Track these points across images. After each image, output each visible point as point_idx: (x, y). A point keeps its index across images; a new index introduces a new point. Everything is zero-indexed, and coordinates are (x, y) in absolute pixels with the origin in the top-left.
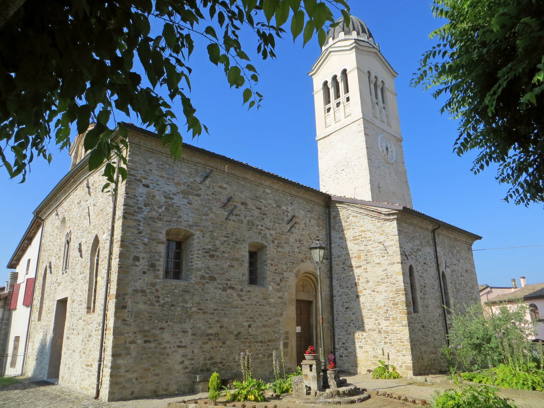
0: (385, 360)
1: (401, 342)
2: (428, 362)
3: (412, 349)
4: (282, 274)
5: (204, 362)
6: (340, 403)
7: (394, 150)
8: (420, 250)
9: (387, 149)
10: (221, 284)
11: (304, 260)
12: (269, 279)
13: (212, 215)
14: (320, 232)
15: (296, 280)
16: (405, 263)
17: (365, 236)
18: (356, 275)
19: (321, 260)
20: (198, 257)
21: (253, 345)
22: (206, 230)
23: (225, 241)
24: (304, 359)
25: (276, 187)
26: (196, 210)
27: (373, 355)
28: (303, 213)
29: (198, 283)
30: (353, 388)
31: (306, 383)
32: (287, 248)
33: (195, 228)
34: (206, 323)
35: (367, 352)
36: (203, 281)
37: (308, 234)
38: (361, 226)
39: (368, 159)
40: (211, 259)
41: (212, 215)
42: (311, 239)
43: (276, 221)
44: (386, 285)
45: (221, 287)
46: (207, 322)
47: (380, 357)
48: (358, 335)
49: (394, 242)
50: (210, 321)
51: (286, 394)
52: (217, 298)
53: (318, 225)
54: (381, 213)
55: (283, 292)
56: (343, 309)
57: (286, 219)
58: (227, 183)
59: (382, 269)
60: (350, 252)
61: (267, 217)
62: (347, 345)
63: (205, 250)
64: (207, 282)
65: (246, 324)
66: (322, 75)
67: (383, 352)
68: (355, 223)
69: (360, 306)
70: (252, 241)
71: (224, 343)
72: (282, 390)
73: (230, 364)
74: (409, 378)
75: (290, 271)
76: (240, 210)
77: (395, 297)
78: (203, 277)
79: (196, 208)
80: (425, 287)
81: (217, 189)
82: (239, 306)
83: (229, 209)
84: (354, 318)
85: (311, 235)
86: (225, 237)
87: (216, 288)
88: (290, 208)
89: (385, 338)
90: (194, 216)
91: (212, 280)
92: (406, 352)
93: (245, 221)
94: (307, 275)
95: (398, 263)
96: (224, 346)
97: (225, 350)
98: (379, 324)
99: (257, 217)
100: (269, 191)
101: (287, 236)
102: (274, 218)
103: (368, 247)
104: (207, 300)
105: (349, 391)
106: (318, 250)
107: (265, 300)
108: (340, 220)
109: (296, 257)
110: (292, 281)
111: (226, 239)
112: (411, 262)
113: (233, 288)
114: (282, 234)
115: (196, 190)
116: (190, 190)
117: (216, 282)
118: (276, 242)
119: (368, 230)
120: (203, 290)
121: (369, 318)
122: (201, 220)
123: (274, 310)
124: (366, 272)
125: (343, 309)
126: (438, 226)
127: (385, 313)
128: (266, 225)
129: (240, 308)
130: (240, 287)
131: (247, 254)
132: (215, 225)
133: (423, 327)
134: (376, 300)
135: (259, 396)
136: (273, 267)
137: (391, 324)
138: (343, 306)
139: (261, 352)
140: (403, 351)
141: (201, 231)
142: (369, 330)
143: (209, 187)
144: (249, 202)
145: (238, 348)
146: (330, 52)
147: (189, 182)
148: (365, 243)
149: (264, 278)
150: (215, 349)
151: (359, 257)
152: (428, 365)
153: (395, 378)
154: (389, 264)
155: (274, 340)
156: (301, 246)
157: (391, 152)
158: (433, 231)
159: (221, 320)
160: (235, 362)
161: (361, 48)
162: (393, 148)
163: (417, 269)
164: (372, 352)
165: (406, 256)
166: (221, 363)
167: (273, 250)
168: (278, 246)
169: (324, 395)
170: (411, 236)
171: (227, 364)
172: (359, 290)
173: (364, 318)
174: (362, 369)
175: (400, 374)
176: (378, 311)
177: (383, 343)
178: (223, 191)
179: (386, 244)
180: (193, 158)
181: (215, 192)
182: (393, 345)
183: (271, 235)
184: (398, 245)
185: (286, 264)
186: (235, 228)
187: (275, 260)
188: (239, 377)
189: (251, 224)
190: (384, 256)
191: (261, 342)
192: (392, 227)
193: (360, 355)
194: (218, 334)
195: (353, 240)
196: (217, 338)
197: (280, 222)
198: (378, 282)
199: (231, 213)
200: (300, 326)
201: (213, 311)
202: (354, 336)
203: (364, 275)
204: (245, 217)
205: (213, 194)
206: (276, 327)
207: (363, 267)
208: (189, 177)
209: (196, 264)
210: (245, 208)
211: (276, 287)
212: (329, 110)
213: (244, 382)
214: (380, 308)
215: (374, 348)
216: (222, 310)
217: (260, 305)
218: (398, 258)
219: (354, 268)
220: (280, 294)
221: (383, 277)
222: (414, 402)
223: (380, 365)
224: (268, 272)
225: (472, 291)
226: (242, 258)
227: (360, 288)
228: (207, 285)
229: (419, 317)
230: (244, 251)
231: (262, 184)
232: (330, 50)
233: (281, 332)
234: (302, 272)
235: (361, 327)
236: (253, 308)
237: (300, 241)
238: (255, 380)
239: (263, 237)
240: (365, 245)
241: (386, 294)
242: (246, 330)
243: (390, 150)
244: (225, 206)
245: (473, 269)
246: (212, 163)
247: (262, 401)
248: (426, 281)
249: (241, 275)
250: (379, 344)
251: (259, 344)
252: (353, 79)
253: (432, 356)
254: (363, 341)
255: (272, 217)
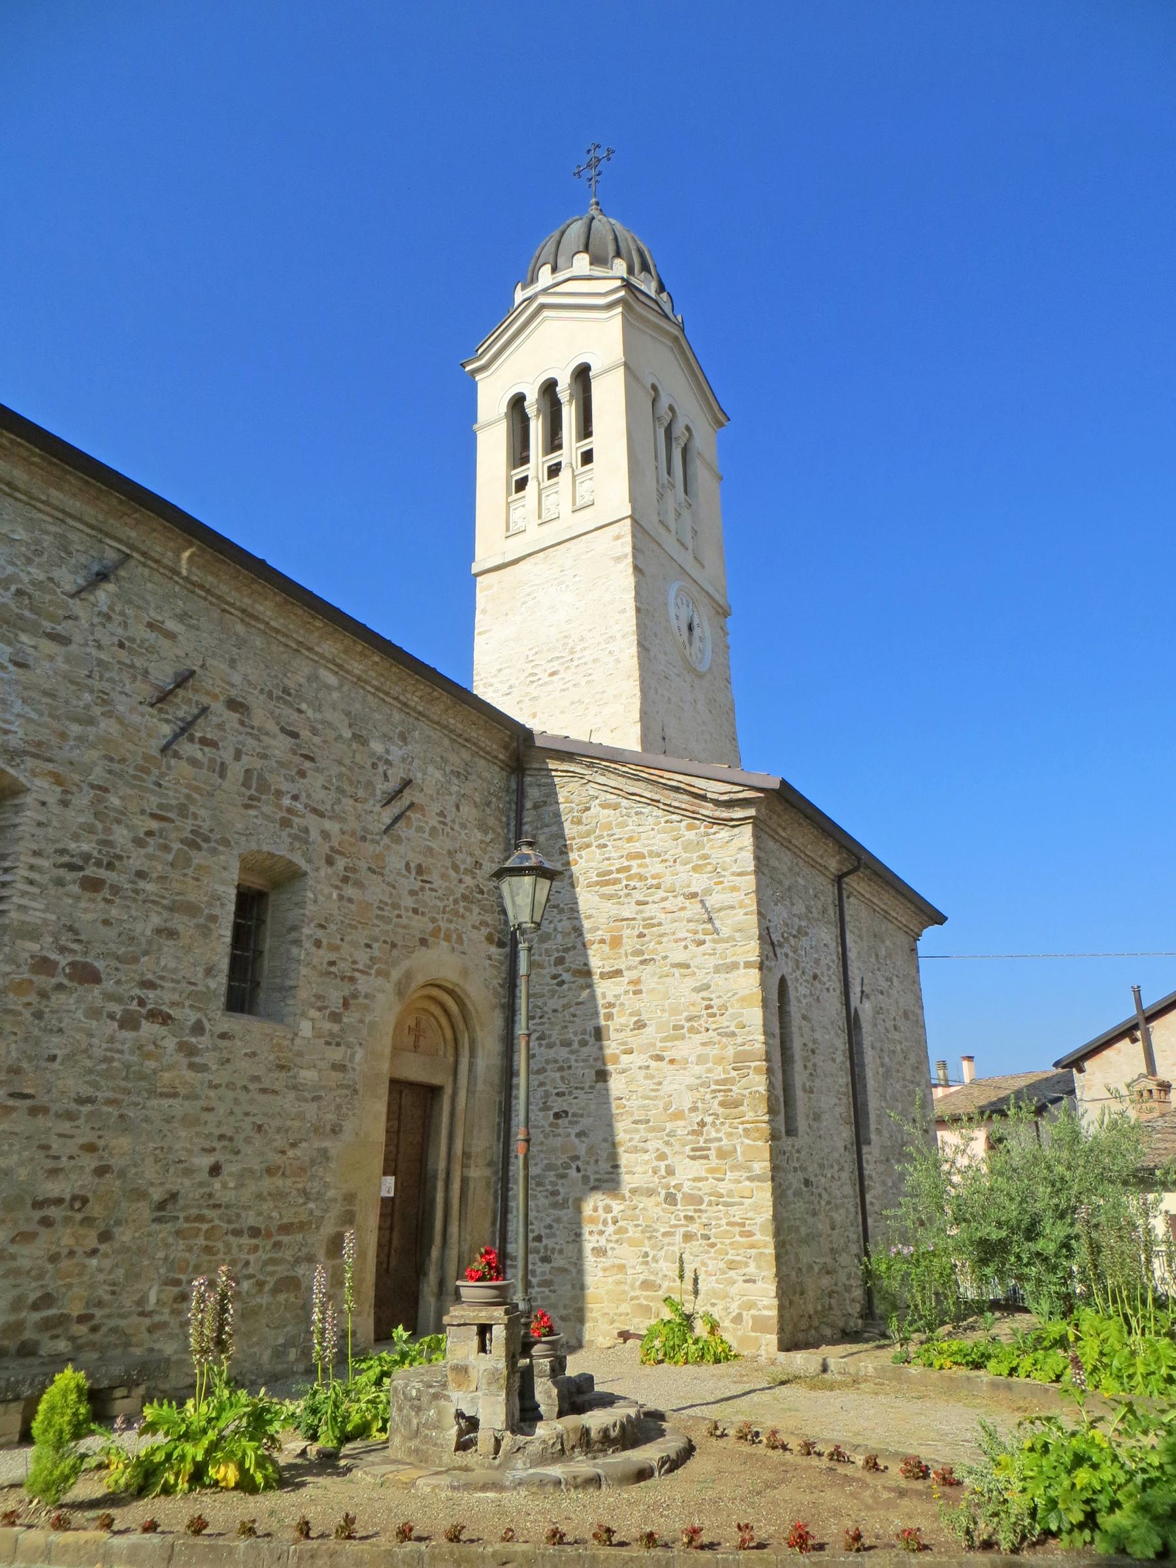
0: (686, 1297)
1: (743, 1234)
2: (839, 1299)
3: (778, 1257)
4: (352, 979)
5: (12, 1318)
6: (595, 1481)
7: (708, 634)
8: (806, 934)
9: (690, 628)
10: (119, 1000)
11: (431, 940)
12: (303, 994)
13: (108, 726)
14: (485, 851)
15: (398, 1008)
16: (770, 969)
17: (642, 871)
18: (601, 1002)
19: (537, 919)
20: (31, 882)
21: (220, 1245)
22: (76, 777)
23: (150, 833)
24: (458, 1297)
25: (357, 667)
26: (45, 693)
27: (642, 1277)
28: (438, 775)
29: (21, 987)
30: (632, 1412)
31: (460, 1399)
32: (376, 891)
33: (30, 762)
34: (39, 1155)
35: (622, 1268)
36: (42, 980)
37: (449, 852)
38: (630, 840)
39: (640, 644)
40: (88, 895)
41: (108, 726)
42: (455, 868)
43: (346, 787)
44: (704, 1037)
45: (117, 1009)
46: (46, 1147)
47: (666, 1284)
48: (594, 1205)
49: (741, 895)
50: (56, 1145)
51: (358, 1443)
52: (98, 1052)
53: (483, 827)
54: (703, 798)
55: (349, 1046)
56: (545, 1118)
57: (381, 787)
58: (182, 617)
59: (691, 983)
60: (587, 924)
61: (317, 770)
62: (550, 1243)
63: (66, 859)
64: (60, 987)
65: (207, 1161)
66: (506, 377)
67: (682, 1270)
68: (608, 826)
69: (609, 1109)
70: (254, 846)
71: (105, 1236)
72: (342, 1430)
73: (122, 1323)
74: (763, 1360)
75: (379, 973)
76: (221, 726)
77: (732, 1081)
78: (44, 965)
79: (47, 686)
80: (813, 1052)
81: (140, 631)
82: (182, 1091)
83: (181, 714)
84: (582, 1148)
85: (459, 856)
86: (154, 816)
87: (94, 1013)
88: (396, 753)
89: (689, 1219)
90: (33, 715)
91: (82, 981)
92: (759, 1267)
93: (236, 770)
94: (435, 992)
95: (748, 965)
96: (103, 1247)
97: (107, 1263)
98: (670, 1172)
99: (281, 764)
100: (332, 680)
101: (379, 849)
102: (340, 776)
103: (650, 910)
104: (53, 1058)
105: (622, 1426)
106: (527, 880)
107: (283, 1074)
108: (557, 815)
109: (405, 927)
110: (385, 1010)
111: (154, 825)
112: (785, 967)
113: (166, 1019)
114: (364, 839)
115: (52, 618)
116: (27, 613)
117: (97, 990)
118: (341, 863)
119: (651, 854)
120: (38, 1015)
121: (635, 1150)
122: (63, 736)
123: (311, 1109)
124: (637, 992)
125: (545, 1118)
126: (856, 861)
127: (693, 1132)
128: (309, 796)
129: (186, 1097)
130: (193, 1017)
131: (231, 895)
132: (116, 767)
133: (807, 1183)
134: (667, 1088)
135: (261, 1463)
136: (321, 952)
137: (712, 1170)
138: (545, 1108)
139: (251, 1271)
140: (746, 1265)
141: (58, 780)
142: (633, 1191)
143: (109, 618)
144: (256, 701)
145: (161, 1255)
146: (543, 307)
147: (26, 579)
148: (638, 895)
149: (287, 991)
150: (65, 1264)
151: (616, 942)
152: (816, 1312)
153: (717, 1361)
154: (717, 969)
155: (302, 1226)
156: (422, 889)
157: (701, 639)
158: (839, 879)
159: (101, 1143)
160: (142, 1314)
161: (638, 308)
162: (705, 629)
163: (798, 991)
164: (639, 1269)
165: (772, 944)
166: (82, 1319)
167: (327, 890)
168: (345, 880)
169: (530, 1448)
170: (787, 883)
171: (112, 1323)
172: (608, 1052)
173: (621, 1150)
174: (598, 1330)
175: (735, 1345)
176: (669, 1126)
177: (678, 1238)
178: (164, 643)
179: (710, 901)
180: (53, 492)
181: (132, 640)
182: (713, 1245)
183: (326, 835)
184: (755, 907)
185: (368, 946)
186: (197, 789)
187: (333, 927)
188: (162, 1381)
189: (256, 787)
190: (704, 942)
191: (255, 1232)
192: (736, 847)
193: (597, 1278)
194: (85, 1201)
195: (597, 883)
196: (79, 1216)
197: (361, 793)
198: (675, 1028)
199: (185, 729)
200: (394, 1174)
201: (73, 1106)
202: (579, 1210)
203: (630, 1001)
204: (238, 755)
205: (121, 645)
206: (313, 1177)
207: (628, 975)
208: (29, 561)
209: (22, 908)
210: (242, 723)
211: (327, 1026)
212: (522, 484)
213: (190, 1404)
214: (678, 1115)
215: (646, 1255)
216: (109, 1102)
217: (264, 1091)
218: (751, 950)
219: (596, 978)
220: (337, 1054)
221: (694, 1011)
222: (872, 1465)
223: (667, 1314)
224: (304, 971)
225: (918, 1078)
226: (210, 905)
227: (611, 1047)
228: (58, 999)
229: (798, 1151)
230: (223, 882)
231: (310, 649)
232: (542, 300)
233: (331, 1193)
234: (420, 979)
235: (608, 1179)
236: (236, 1101)
237: (420, 870)
238: (242, 1394)
239: (295, 838)
240: (639, 903)
241: (698, 1069)
242: (201, 1184)
243: (697, 632)
244: (163, 698)
245: (919, 1012)
246: (132, 530)
247: (268, 1487)
248: (817, 1035)
249: (200, 970)
250: (667, 1240)
251: (245, 1240)
252: (610, 398)
253: (825, 1281)
254: (611, 1229)
255: (335, 770)
